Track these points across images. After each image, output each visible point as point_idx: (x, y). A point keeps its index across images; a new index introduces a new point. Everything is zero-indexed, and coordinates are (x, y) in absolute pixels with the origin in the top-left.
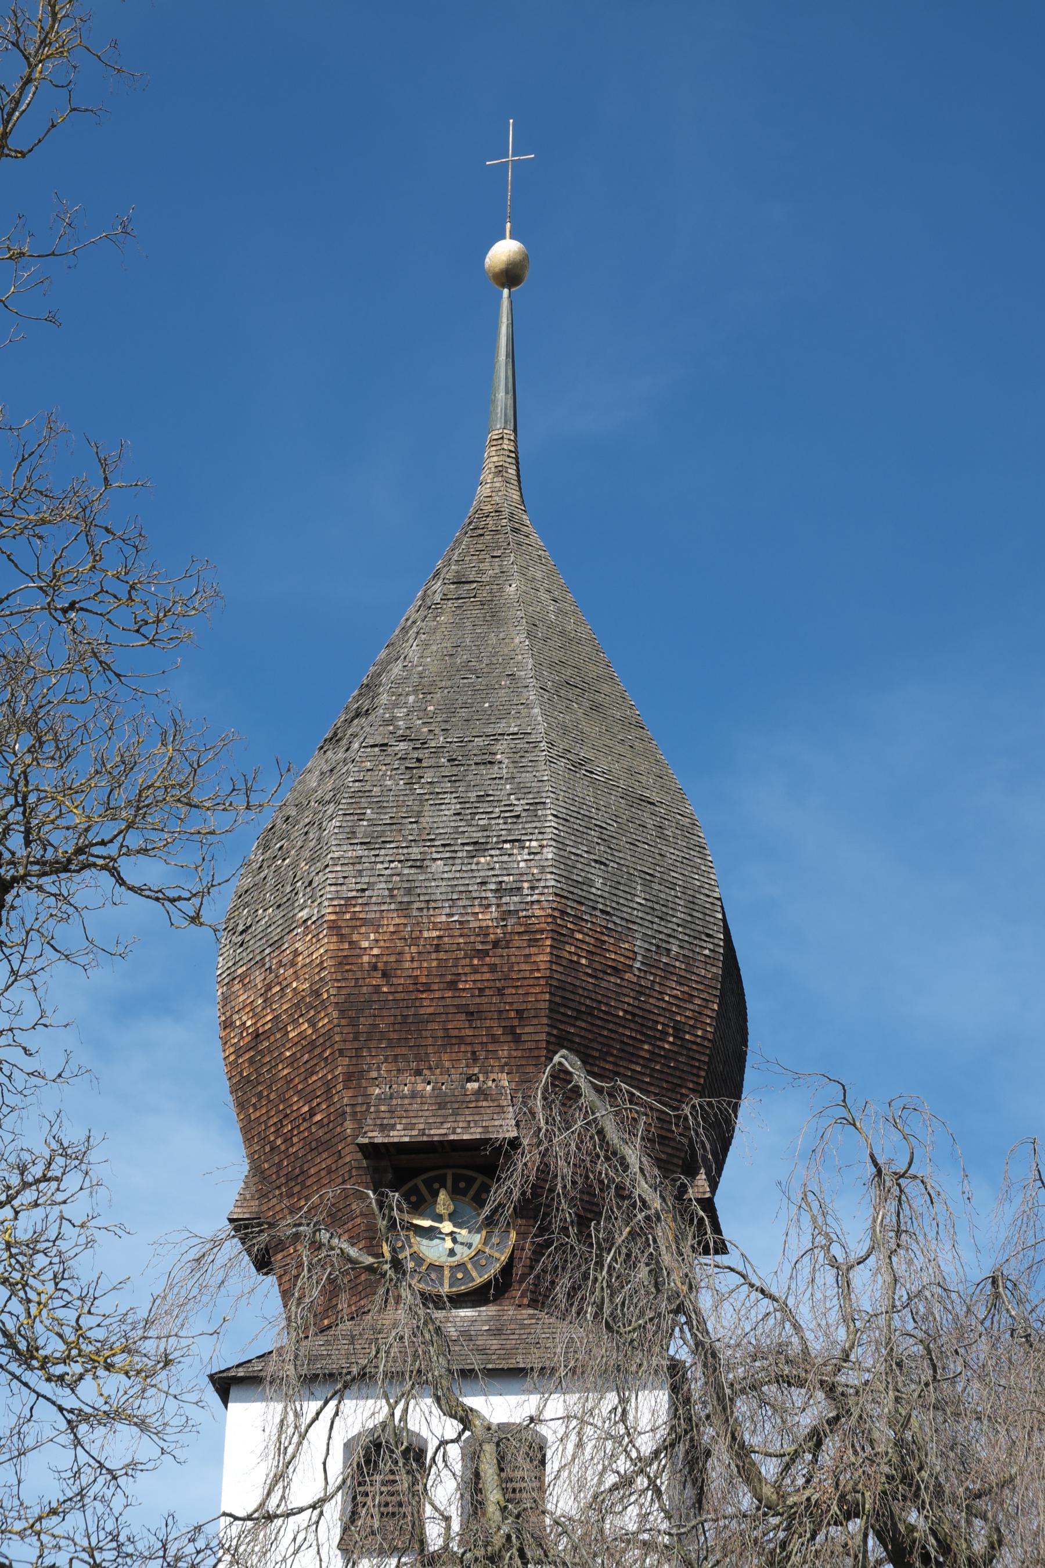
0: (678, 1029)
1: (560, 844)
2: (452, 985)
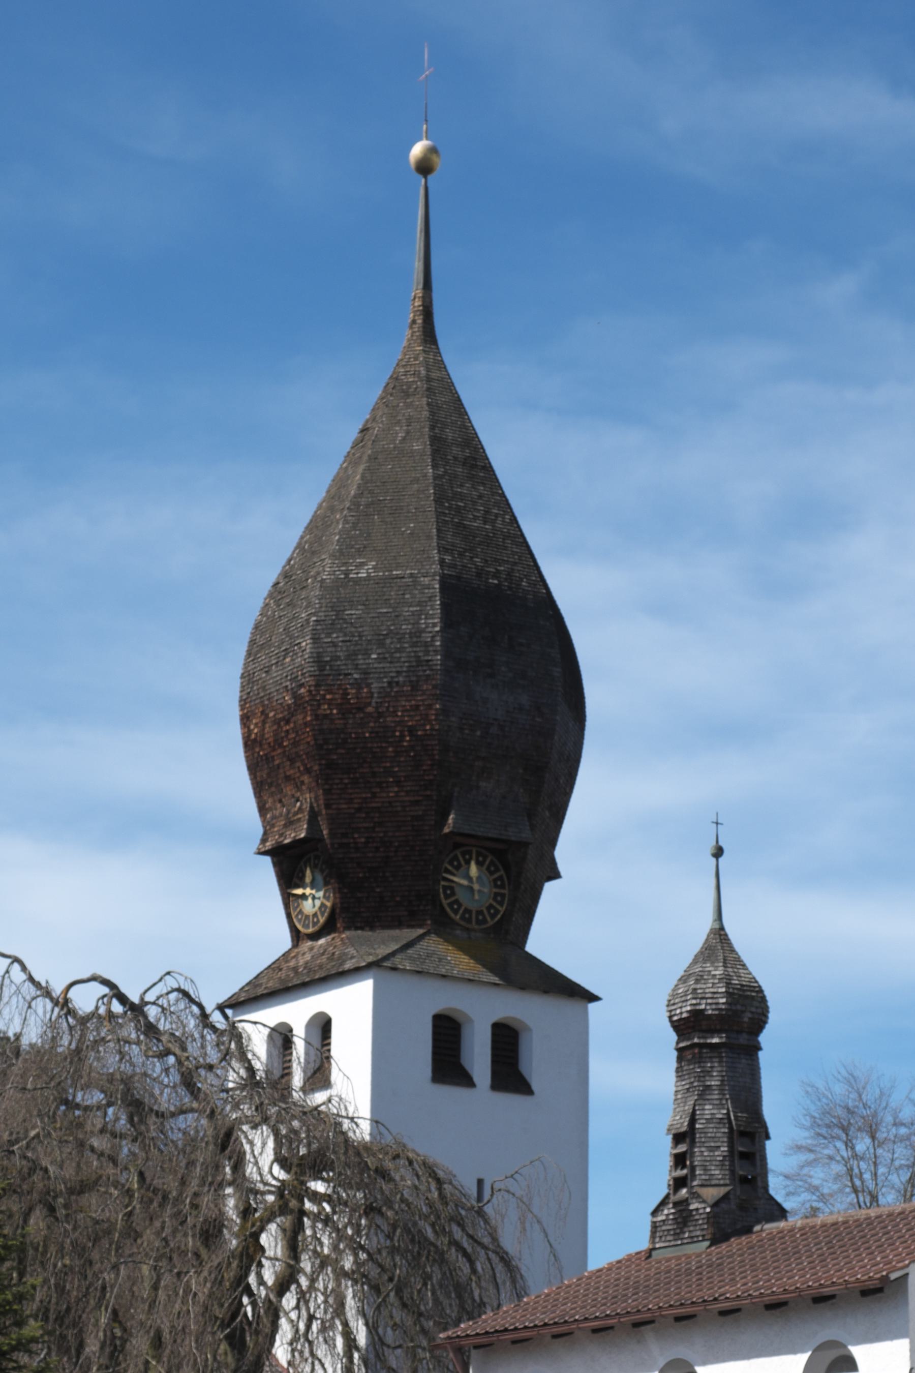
0: (411, 731)
1: (316, 639)
2: (280, 745)
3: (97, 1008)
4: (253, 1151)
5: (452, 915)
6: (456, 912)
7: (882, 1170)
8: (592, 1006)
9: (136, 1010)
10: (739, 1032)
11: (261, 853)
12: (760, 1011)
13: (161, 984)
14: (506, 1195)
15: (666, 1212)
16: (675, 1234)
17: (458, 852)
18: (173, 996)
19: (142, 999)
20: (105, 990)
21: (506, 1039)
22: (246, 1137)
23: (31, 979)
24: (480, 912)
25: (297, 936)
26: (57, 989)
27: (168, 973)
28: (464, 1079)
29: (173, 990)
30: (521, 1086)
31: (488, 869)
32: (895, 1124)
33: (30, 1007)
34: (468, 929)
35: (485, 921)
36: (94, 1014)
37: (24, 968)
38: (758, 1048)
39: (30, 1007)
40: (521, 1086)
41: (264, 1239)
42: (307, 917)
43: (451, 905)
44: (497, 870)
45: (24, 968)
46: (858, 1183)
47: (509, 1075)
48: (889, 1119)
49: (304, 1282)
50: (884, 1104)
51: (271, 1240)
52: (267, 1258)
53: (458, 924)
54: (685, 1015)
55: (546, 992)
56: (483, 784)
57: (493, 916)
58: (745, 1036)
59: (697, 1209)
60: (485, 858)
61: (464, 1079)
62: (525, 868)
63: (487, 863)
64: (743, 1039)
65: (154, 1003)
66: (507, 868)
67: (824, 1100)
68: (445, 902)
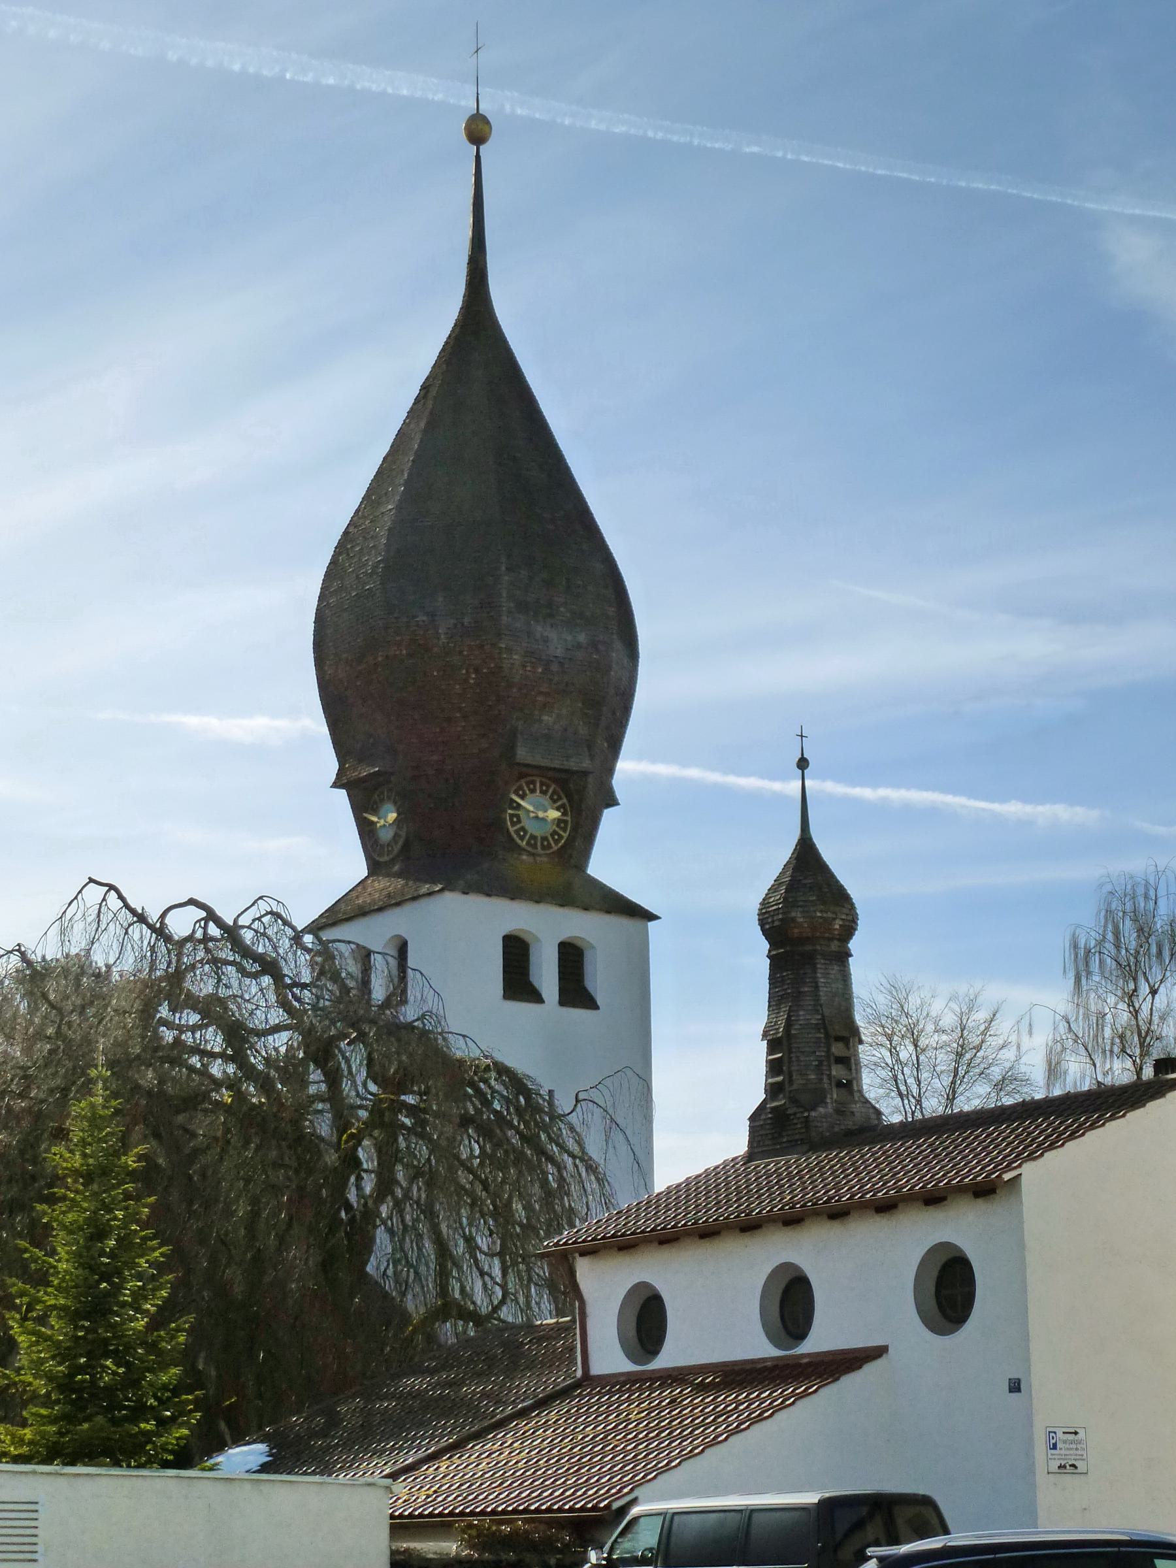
3: (194, 931)
4: (350, 1067)
5: (519, 842)
6: (522, 838)
7: (925, 1075)
8: (651, 924)
9: (231, 933)
10: (831, 939)
11: (335, 785)
12: (850, 918)
13: (255, 907)
14: (590, 1104)
15: (763, 1117)
16: (773, 1138)
17: (523, 782)
18: (266, 920)
19: (236, 921)
20: (204, 914)
21: (572, 958)
22: (344, 1057)
23: (127, 906)
24: (544, 839)
25: (375, 867)
26: (154, 917)
27: (261, 898)
28: (535, 996)
29: (267, 913)
30: (590, 1003)
31: (551, 798)
32: (936, 1031)
33: (126, 933)
34: (533, 855)
35: (549, 846)
36: (190, 938)
37: (121, 897)
38: (848, 954)
39: (126, 933)
40: (590, 1003)
41: (361, 1153)
42: (382, 846)
43: (517, 832)
44: (560, 798)
45: (121, 897)
46: (903, 1088)
47: (575, 992)
48: (930, 1027)
49: (399, 1193)
50: (925, 1014)
51: (366, 1155)
52: (366, 1171)
53: (524, 850)
54: (777, 923)
55: (608, 912)
56: (545, 718)
57: (556, 842)
58: (836, 942)
59: (795, 1114)
60: (548, 787)
61: (535, 996)
62: (586, 796)
63: (551, 791)
64: (834, 946)
65: (249, 927)
66: (569, 796)
67: (868, 1010)
68: (512, 830)
